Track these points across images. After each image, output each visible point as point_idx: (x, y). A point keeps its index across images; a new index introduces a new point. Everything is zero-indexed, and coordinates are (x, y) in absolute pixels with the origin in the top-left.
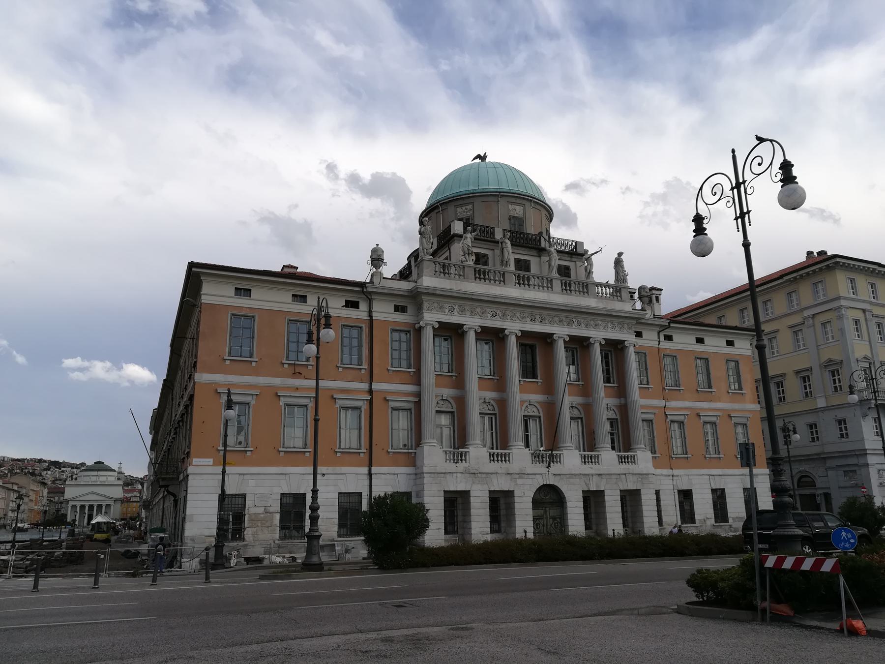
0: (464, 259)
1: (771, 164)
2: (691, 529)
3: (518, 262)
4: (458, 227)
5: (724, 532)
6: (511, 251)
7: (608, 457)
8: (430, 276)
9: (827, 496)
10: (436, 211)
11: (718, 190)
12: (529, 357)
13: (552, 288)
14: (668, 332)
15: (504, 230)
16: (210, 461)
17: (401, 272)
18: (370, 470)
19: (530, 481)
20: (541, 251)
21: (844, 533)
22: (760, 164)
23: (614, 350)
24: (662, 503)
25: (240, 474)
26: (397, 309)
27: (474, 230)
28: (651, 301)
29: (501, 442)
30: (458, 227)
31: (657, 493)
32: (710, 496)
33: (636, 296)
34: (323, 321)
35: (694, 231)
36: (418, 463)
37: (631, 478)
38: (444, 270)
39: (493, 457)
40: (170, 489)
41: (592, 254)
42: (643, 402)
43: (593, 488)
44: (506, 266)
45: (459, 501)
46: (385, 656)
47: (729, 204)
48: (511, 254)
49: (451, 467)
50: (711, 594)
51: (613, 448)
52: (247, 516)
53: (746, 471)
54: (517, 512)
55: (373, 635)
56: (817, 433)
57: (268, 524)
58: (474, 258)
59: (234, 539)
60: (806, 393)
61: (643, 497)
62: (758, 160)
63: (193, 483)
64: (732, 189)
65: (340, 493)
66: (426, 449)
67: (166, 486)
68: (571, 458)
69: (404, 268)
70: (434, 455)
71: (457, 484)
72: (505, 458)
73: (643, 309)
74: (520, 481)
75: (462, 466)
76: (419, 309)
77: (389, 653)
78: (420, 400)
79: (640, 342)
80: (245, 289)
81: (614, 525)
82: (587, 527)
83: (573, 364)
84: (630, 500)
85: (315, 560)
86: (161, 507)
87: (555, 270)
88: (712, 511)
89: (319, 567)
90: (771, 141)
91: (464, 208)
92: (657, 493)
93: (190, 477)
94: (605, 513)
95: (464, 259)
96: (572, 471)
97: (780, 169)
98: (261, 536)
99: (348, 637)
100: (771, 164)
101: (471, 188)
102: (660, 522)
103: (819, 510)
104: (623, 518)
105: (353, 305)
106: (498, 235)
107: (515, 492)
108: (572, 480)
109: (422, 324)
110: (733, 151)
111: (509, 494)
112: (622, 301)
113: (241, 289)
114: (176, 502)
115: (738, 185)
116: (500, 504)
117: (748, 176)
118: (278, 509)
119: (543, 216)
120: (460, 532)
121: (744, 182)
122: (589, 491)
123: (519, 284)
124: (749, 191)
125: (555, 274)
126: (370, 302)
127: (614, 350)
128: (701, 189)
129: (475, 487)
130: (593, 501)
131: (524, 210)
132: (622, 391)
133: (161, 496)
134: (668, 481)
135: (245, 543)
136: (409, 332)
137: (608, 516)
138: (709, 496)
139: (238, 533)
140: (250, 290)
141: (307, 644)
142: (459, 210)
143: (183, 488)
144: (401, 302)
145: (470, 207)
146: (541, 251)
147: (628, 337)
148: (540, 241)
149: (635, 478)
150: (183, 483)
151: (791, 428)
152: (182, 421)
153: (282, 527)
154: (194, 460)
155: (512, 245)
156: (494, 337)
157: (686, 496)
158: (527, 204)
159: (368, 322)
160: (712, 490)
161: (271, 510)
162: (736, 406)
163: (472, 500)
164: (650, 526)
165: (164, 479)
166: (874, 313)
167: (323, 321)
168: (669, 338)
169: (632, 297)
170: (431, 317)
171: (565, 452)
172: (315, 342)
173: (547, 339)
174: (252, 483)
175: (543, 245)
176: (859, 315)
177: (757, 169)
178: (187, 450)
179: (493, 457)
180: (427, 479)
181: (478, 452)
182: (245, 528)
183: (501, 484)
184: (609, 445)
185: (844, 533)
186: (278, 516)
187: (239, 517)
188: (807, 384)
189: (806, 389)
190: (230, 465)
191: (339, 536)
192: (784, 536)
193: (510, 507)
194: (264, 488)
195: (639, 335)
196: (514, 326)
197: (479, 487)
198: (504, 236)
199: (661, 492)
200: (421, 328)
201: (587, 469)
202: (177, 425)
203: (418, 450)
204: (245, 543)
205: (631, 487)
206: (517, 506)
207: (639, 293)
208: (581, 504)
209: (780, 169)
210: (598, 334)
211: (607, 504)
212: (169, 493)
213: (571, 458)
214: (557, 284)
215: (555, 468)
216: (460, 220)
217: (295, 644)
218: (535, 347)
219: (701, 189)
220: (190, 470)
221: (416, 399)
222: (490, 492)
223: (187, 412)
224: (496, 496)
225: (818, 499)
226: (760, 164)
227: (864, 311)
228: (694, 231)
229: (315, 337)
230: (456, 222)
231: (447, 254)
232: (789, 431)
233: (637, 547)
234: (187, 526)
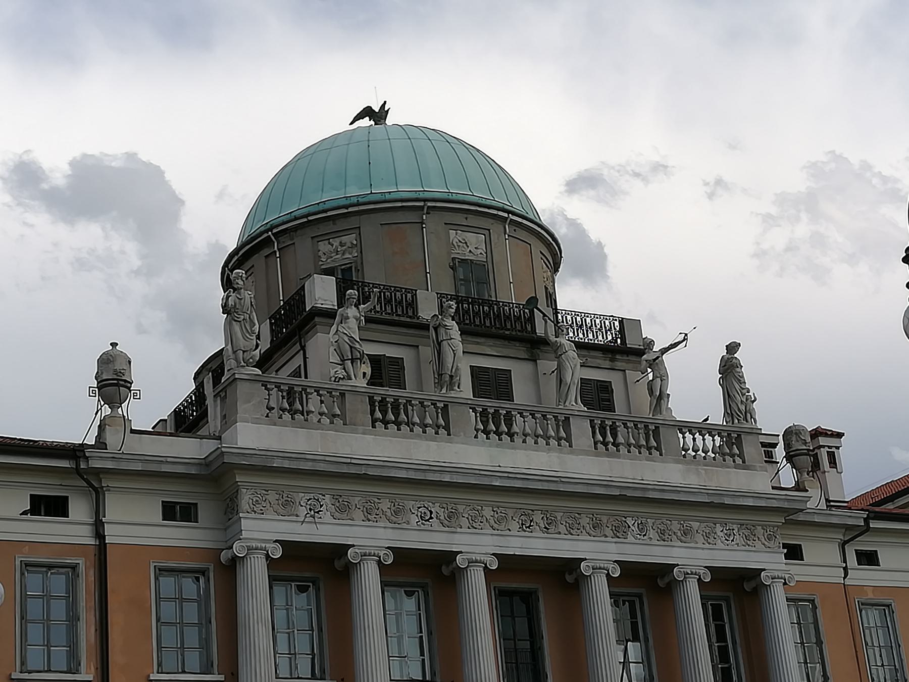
0: (341, 373)
6: (460, 348)
8: (256, 421)
10: (266, 251)
12: (522, 625)
14: (865, 544)
15: (441, 296)
17: (177, 413)
20: (535, 346)
23: (736, 593)
28: (816, 465)
30: (322, 292)
33: (780, 452)
38: (293, 403)
41: (664, 351)
44: (451, 387)
48: (462, 357)
58: (367, 368)
69: (188, 403)
79: (797, 571)
83: (636, 639)
87: (574, 393)
91: (336, 242)
95: (341, 373)
106: (427, 310)
109: (238, 549)
112: (745, 466)
125: (574, 404)
127: (736, 593)
131: (489, 242)
136: (203, 572)
142: (324, 247)
144: (180, 495)
145: (350, 239)
146: (535, 346)
147: (767, 560)
155: (463, 332)
158: (496, 229)
159: (92, 552)
168: (869, 559)
169: (769, 455)
170: (263, 529)
173: (565, 575)
175: (540, 331)
195: (794, 553)
196: (478, 544)
200: (234, 560)
207: (787, 446)
210: (694, 556)
214: (581, 431)
216: (329, 272)
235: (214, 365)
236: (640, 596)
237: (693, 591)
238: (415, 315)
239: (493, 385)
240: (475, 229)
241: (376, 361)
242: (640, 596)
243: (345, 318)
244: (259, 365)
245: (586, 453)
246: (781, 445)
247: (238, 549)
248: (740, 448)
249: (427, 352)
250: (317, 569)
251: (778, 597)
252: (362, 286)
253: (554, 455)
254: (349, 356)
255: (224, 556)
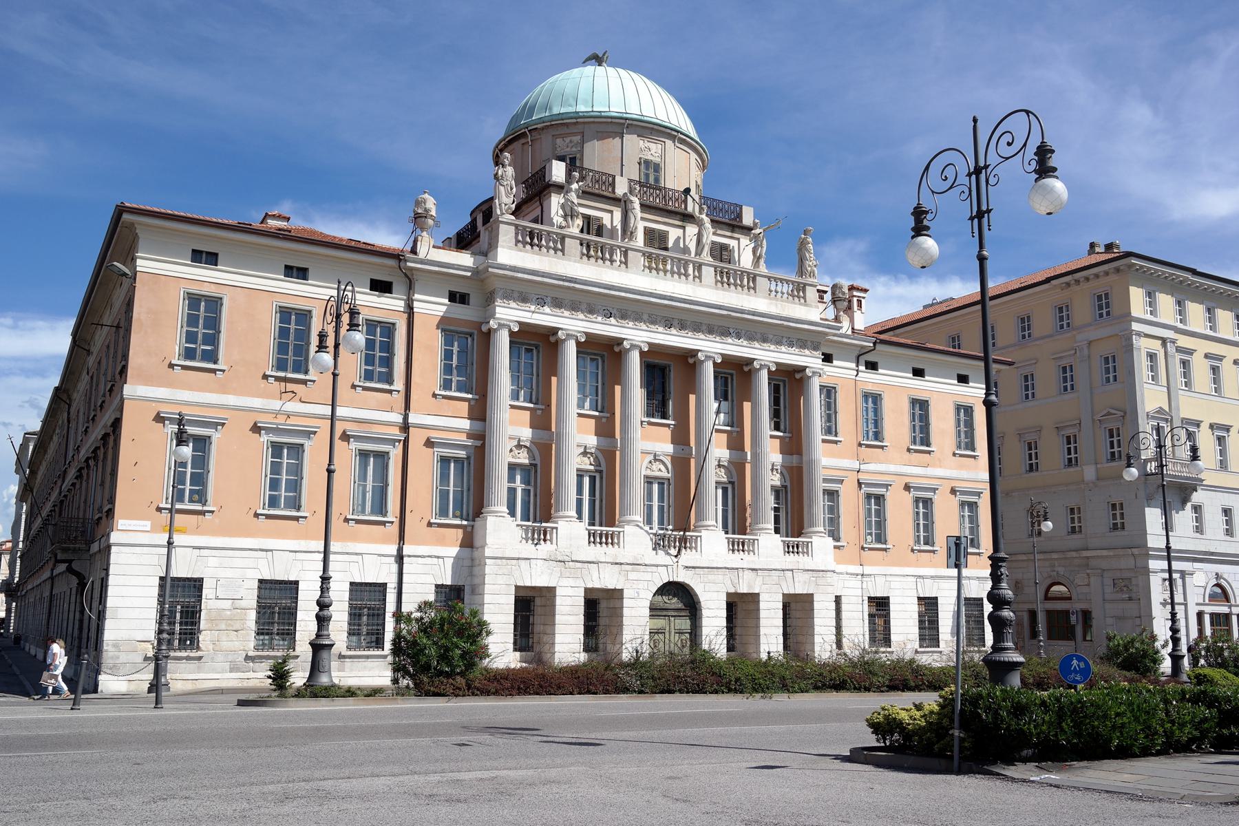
0: (564, 224)
1: (1025, 145)
2: (885, 655)
3: (649, 233)
4: (558, 171)
5: (931, 659)
7: (769, 543)
8: (510, 248)
9: (1086, 616)
10: (523, 141)
11: (950, 172)
12: (657, 383)
13: (700, 277)
14: (870, 357)
15: (630, 180)
16: (147, 525)
17: (459, 235)
18: (400, 550)
19: (648, 576)
21: (1075, 662)
22: (1009, 144)
23: (789, 382)
24: (844, 615)
25: (195, 548)
26: (453, 297)
27: (582, 178)
28: (850, 307)
29: (604, 514)
30: (558, 171)
31: (838, 600)
32: (916, 608)
33: (828, 297)
34: (345, 319)
35: (913, 229)
36: (477, 543)
37: (800, 577)
38: (531, 239)
39: (593, 538)
40: (75, 566)
42: (829, 460)
43: (743, 589)
44: (630, 239)
45: (538, 601)
46: (459, 801)
47: (964, 196)
48: (640, 223)
49: (528, 549)
50: (896, 736)
51: (777, 531)
52: (203, 613)
53: (954, 572)
54: (626, 621)
55: (437, 777)
56: (1122, 518)
57: (237, 626)
58: (579, 222)
59: (183, 646)
60: (1070, 460)
61: (816, 605)
62: (1008, 138)
63: (119, 560)
64: (969, 175)
65: (352, 584)
66: (491, 521)
67: (70, 562)
68: (712, 542)
69: (466, 229)
70: (502, 531)
71: (537, 578)
72: (608, 539)
73: (837, 319)
74: (632, 576)
75: (545, 549)
76: (489, 300)
77: (462, 797)
78: (483, 445)
79: (828, 369)
80: (208, 253)
81: (770, 641)
82: (730, 648)
83: (726, 399)
84: (797, 610)
85: (324, 680)
86: (47, 594)
87: (707, 249)
88: (916, 630)
89: (330, 692)
90: (1028, 112)
91: (568, 140)
92: (838, 600)
93: (113, 549)
94: (758, 627)
95: (564, 224)
96: (714, 564)
97: (1036, 154)
98: (225, 644)
99: (401, 778)
100: (1025, 145)
101: (582, 108)
102: (839, 644)
103: (385, 515)
104: (785, 635)
105: (381, 287)
106: (621, 189)
107: (625, 592)
108: (711, 577)
109: (493, 324)
110: (975, 120)
111: (615, 595)
112: (806, 304)
113: (201, 252)
114: (82, 585)
115: (978, 171)
116: (600, 609)
117: (993, 159)
118: (254, 604)
119: (693, 162)
120: (537, 648)
121: (986, 167)
122: (736, 594)
123: (650, 268)
124: (992, 181)
125: (706, 257)
126: (410, 288)
127: (789, 382)
128: (927, 168)
129: (564, 582)
130: (740, 608)
132: (794, 445)
133: (47, 574)
134: (856, 582)
135: (199, 654)
136: (471, 335)
137: (763, 631)
138: (913, 609)
139: (190, 637)
140: (216, 255)
141: (344, 785)
142: (559, 141)
143: (98, 565)
144: (460, 288)
145: (577, 138)
147: (809, 360)
148: (685, 201)
149: (807, 575)
150: (98, 557)
151: (1042, 513)
152: (95, 458)
153: (259, 633)
154: (121, 522)
155: (642, 205)
156: (604, 356)
157: (880, 606)
158: (669, 143)
160: (919, 599)
161: (243, 604)
162: (964, 474)
163: (558, 601)
164: (823, 647)
165: (65, 550)
166: (1179, 344)
167: (345, 319)
168: (872, 366)
169: (821, 297)
170: (509, 314)
171: (704, 533)
172: (331, 349)
173: (688, 360)
174: (213, 562)
175: (690, 209)
176: (1156, 346)
177: (1006, 151)
178: (109, 506)
179: (593, 538)
180: (490, 568)
181: (571, 530)
182: (199, 631)
183: (605, 579)
184: (771, 526)
185: (1075, 662)
186: (253, 615)
187: (191, 616)
188: (1072, 446)
189: (1069, 453)
190: (180, 531)
191: (349, 648)
192: (1000, 662)
193: (617, 613)
194: (231, 569)
195: (828, 358)
196: (638, 336)
197: (571, 582)
198: (631, 191)
199: (844, 600)
200: (489, 330)
201: (736, 559)
202: (84, 465)
203: (478, 522)
204: (199, 654)
205: (800, 589)
206: (626, 612)
207: (833, 294)
208: (723, 613)
209: (1036, 154)
210: (767, 355)
211: (763, 614)
212: (70, 570)
213: (712, 542)
214: (708, 272)
215: (688, 557)
216: (561, 159)
217: (328, 784)
218: (667, 377)
219: (927, 168)
220: (114, 537)
221: (479, 443)
222: (586, 590)
223: (105, 445)
224: (594, 596)
225: (1073, 619)
226: (1009, 144)
227: (1164, 341)
228: (913, 229)
229: (330, 342)
230: (555, 162)
231: (538, 212)
232: (1038, 516)
233: (799, 674)
234: (109, 624)
235: (484, 208)
236: (732, 375)
237: (764, 375)
238: (614, 192)
239: (656, 239)
240: (656, 142)
241: (587, 219)
242: (732, 375)
243: (570, 190)
244: (512, 214)
245: (708, 286)
246: (829, 293)
247: (493, 324)
248: (804, 292)
249: (618, 214)
250: (537, 346)
251: (815, 384)
252: (582, 168)
253: (689, 286)
254: (569, 214)
255: (484, 329)
